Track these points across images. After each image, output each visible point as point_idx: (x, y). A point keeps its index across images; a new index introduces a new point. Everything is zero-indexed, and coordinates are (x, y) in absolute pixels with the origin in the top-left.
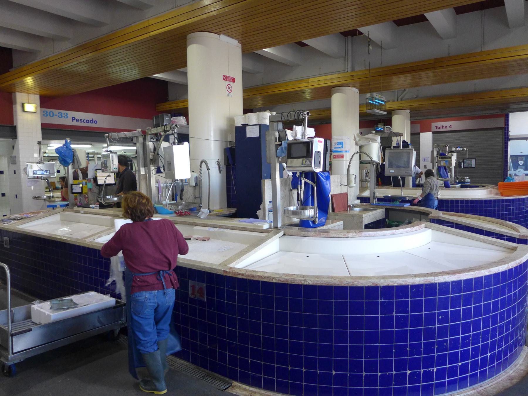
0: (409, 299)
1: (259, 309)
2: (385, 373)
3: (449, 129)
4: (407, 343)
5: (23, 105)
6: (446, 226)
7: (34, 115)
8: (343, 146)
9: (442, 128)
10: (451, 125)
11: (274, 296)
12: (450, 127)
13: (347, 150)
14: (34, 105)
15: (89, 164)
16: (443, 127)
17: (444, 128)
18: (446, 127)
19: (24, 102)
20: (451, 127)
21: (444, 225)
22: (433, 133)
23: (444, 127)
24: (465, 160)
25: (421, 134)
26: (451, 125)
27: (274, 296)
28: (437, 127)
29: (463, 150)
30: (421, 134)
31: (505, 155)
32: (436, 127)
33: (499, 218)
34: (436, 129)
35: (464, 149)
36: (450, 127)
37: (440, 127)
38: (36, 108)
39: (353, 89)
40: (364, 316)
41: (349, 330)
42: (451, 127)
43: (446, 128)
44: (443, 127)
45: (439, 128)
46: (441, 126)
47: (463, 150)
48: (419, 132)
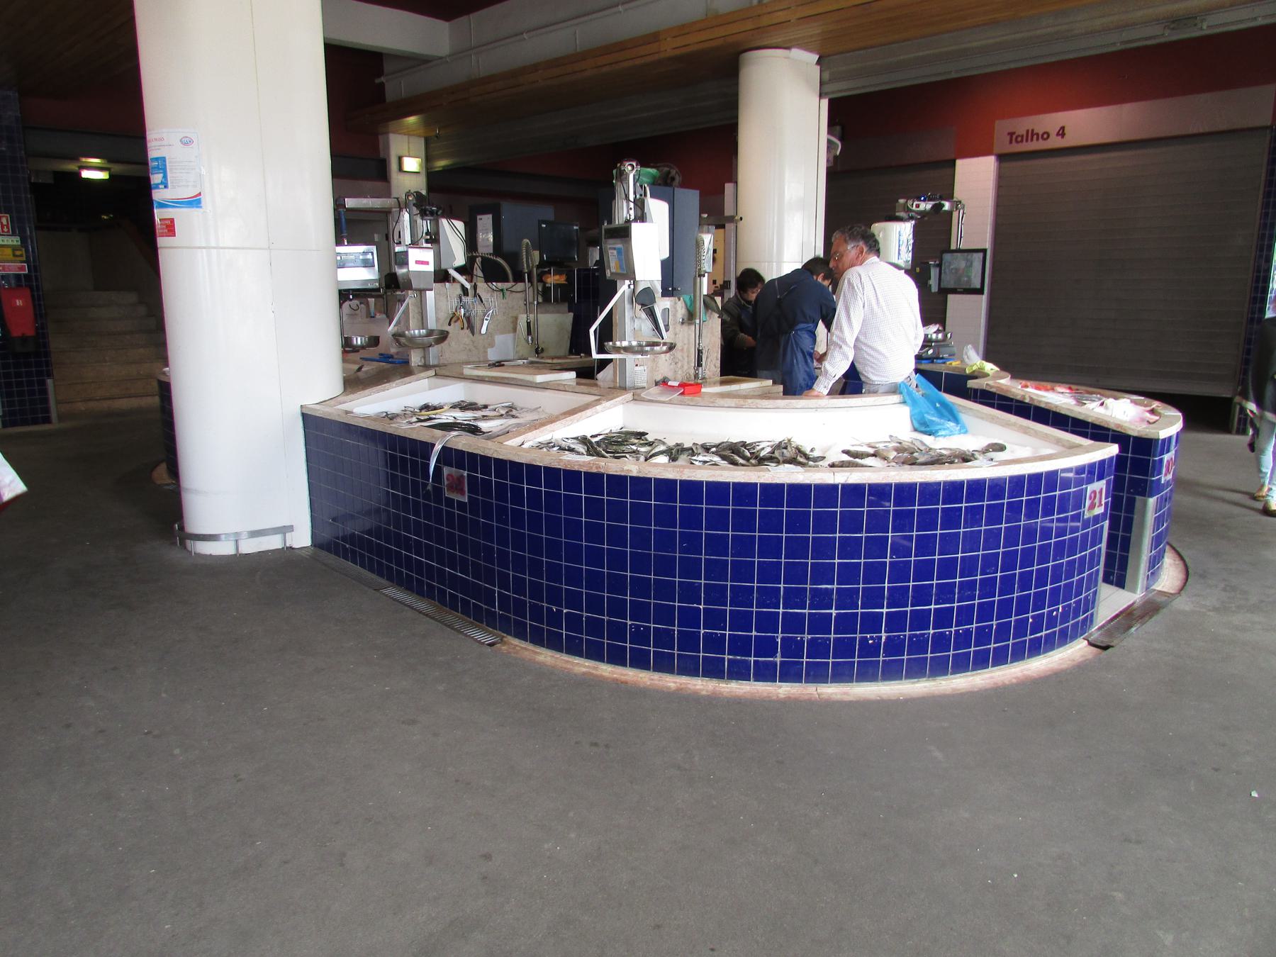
0: (704, 532)
1: (507, 529)
2: (763, 634)
3: (1055, 142)
4: (881, 610)
5: (400, 159)
6: (1073, 432)
7: (414, 177)
8: (165, 177)
9: (1032, 140)
10: (1063, 128)
11: (584, 519)
12: (1058, 134)
13: (188, 193)
14: (418, 160)
15: (719, 317)
16: (1035, 137)
17: (1038, 139)
18: (1045, 136)
19: (401, 154)
20: (1062, 133)
21: (1067, 431)
22: (1002, 158)
23: (1038, 134)
24: (947, 257)
25: (959, 163)
26: (1063, 128)
27: (584, 519)
28: (1014, 137)
29: (938, 208)
30: (962, 166)
31: (1264, 235)
32: (1011, 134)
33: (976, 402)
34: (1011, 142)
35: (943, 206)
36: (1058, 134)
37: (1022, 136)
38: (421, 165)
39: (796, 53)
40: (677, 555)
41: (755, 585)
42: (1063, 135)
43: (1046, 136)
44: (1035, 137)
45: (1019, 139)
46: (1028, 131)
47: (938, 208)
48: (952, 156)
